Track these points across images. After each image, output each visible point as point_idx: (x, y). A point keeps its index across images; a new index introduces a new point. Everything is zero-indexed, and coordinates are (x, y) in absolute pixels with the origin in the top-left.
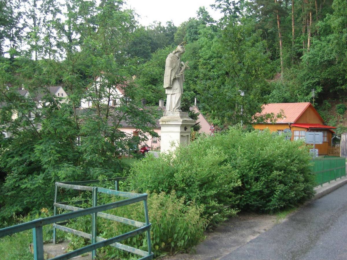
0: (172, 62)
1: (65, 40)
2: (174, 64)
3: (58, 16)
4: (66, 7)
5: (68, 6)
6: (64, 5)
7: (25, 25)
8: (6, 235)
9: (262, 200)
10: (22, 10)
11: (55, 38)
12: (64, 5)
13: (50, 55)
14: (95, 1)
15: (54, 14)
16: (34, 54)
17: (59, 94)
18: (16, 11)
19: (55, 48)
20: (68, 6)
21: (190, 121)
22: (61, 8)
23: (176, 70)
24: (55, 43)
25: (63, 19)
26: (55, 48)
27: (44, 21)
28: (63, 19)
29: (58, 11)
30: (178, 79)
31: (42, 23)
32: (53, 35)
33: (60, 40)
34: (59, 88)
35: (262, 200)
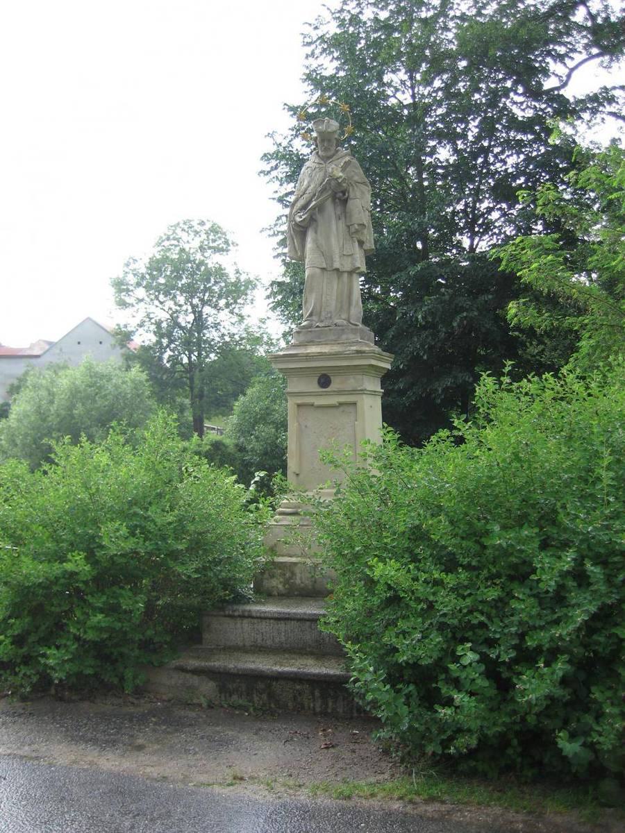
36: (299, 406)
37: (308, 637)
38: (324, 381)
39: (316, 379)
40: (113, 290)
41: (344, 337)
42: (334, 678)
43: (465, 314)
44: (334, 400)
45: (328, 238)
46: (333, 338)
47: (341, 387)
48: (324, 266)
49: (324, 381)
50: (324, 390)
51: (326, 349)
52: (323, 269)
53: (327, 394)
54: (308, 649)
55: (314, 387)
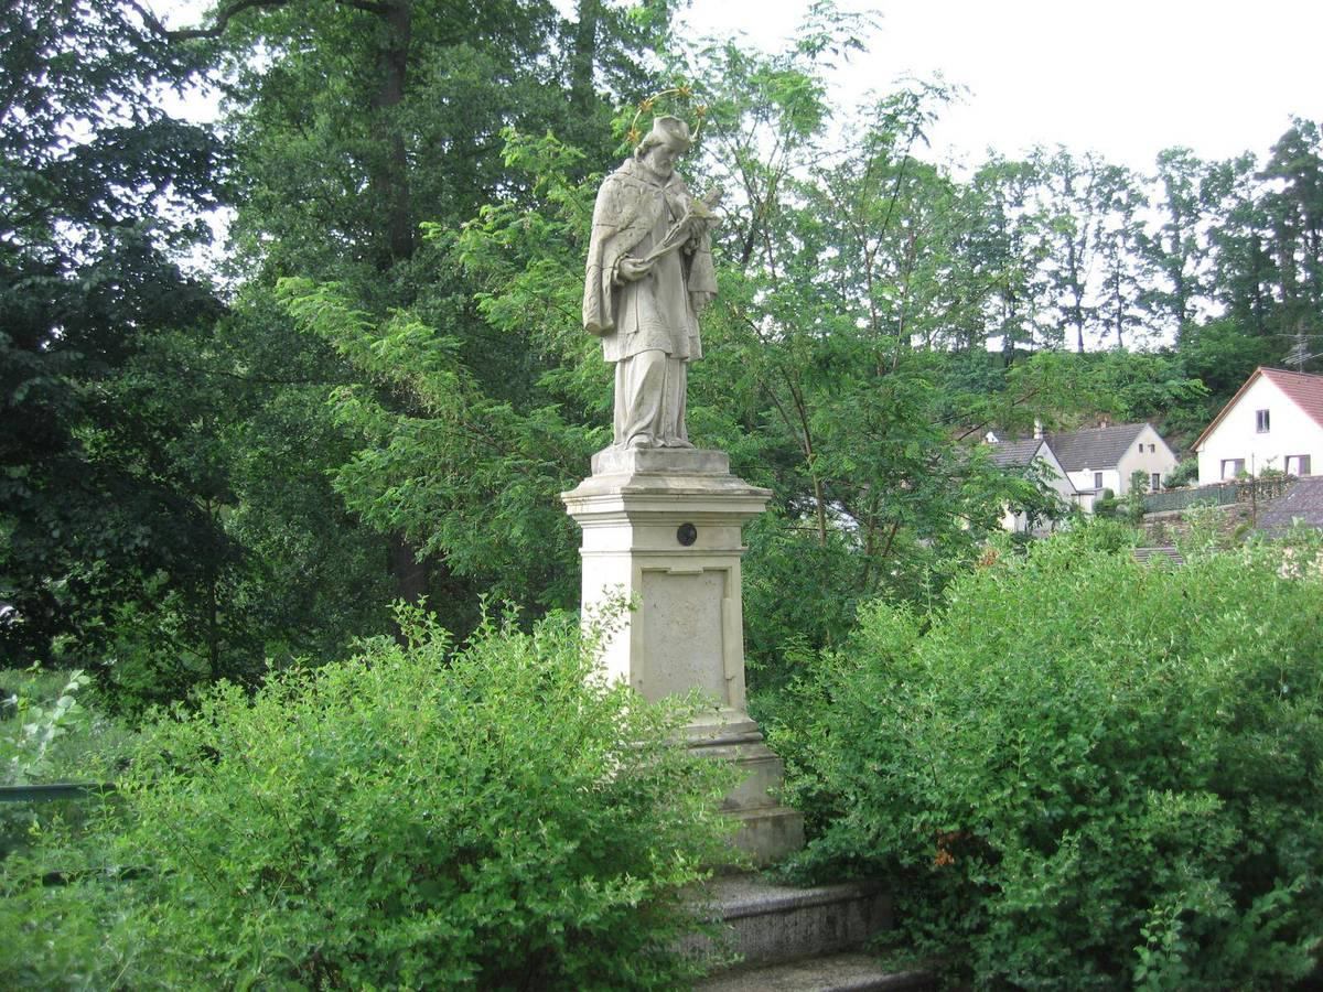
0: (614, 204)
1: (1164, 283)
2: (627, 211)
3: (1140, 213)
4: (1161, 185)
5: (1169, 179)
6: (1154, 180)
7: (1042, 252)
8: (989, 847)
9: (1088, 967)
10: (1030, 209)
11: (1133, 280)
12: (1154, 180)
13: (1120, 332)
14: (1254, 156)
15: (1127, 210)
16: (1071, 331)
17: (1141, 446)
18: (1012, 214)
19: (1134, 311)
20: (1169, 179)
21: (701, 492)
22: (1145, 190)
23: (627, 240)
24: (1133, 297)
25: (1155, 220)
26: (1134, 311)
27: (1097, 235)
28: (1155, 220)
29: (1138, 199)
30: (648, 278)
31: (1091, 241)
32: (1126, 273)
33: (1147, 287)
34: (1140, 430)
35: (1088, 967)
36: (644, 572)
37: (767, 939)
38: (687, 535)
39: (675, 530)
40: (1240, 155)
41: (709, 466)
42: (883, 988)
43: (38, 381)
44: (697, 565)
45: (671, 306)
46: (694, 466)
47: (716, 545)
48: (670, 350)
49: (687, 535)
50: (690, 548)
51: (692, 485)
52: (668, 355)
53: (692, 555)
54: (765, 959)
55: (672, 544)
